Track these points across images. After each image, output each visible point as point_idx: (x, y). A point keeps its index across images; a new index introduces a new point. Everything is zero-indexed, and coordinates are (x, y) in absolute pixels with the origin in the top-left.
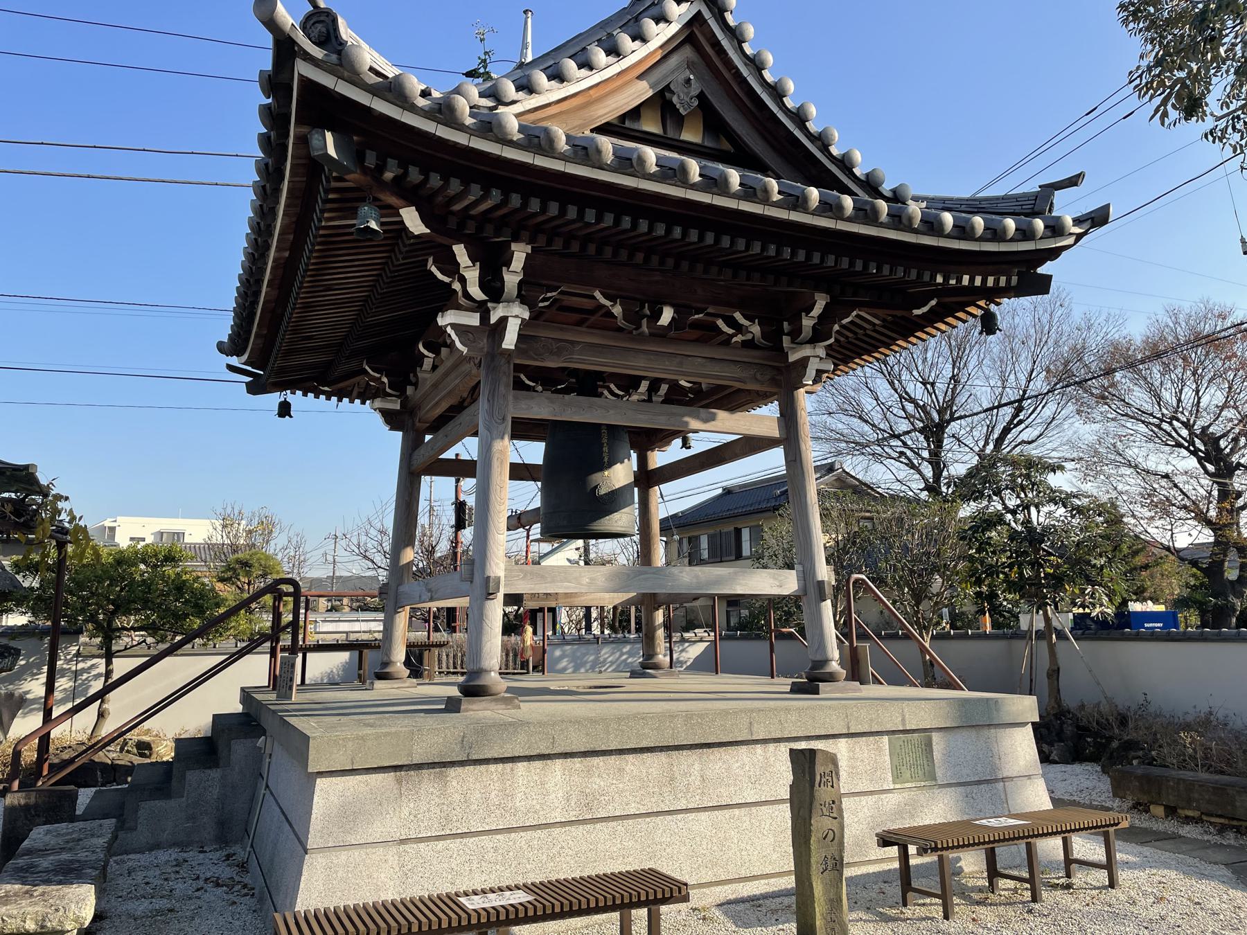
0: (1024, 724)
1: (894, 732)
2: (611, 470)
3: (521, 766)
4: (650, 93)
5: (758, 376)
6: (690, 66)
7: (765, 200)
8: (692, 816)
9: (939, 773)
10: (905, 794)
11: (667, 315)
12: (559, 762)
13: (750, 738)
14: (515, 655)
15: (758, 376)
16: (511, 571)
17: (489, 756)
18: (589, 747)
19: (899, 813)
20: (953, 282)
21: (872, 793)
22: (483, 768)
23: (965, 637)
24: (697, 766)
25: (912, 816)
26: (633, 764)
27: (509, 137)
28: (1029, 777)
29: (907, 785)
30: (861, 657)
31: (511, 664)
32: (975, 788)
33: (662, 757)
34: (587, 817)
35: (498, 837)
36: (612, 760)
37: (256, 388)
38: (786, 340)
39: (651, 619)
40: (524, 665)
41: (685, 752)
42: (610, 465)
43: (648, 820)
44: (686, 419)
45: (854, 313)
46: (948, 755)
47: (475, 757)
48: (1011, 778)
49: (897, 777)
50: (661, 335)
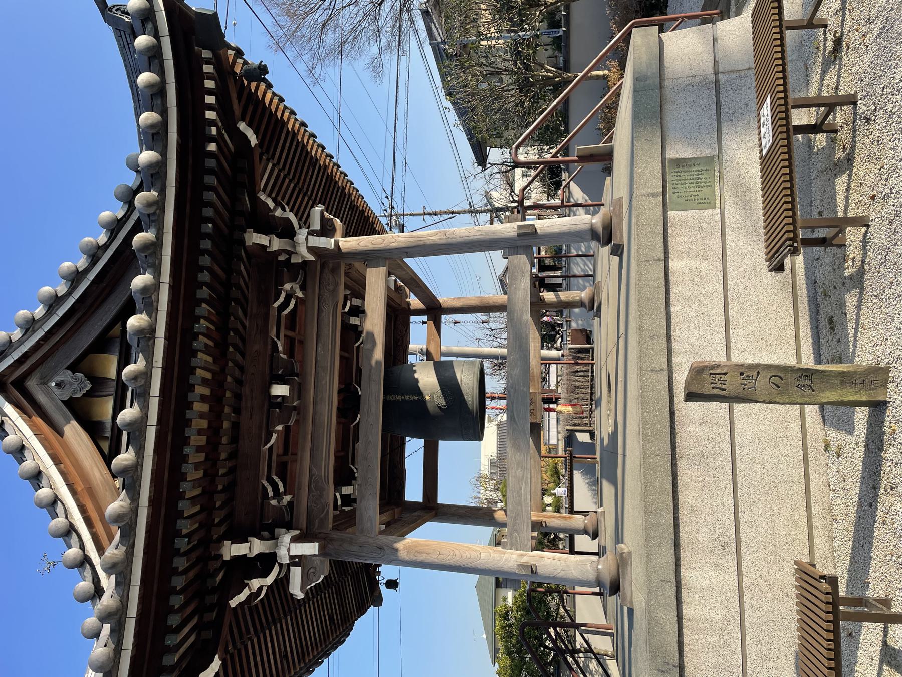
0: (660, 37)
1: (665, 204)
2: (425, 392)
3: (686, 611)
4: (74, 423)
5: (331, 287)
6: (44, 381)
7: (146, 375)
8: (738, 439)
9: (706, 152)
10: (727, 195)
11: (280, 390)
12: (683, 573)
13: (666, 373)
14: (579, 358)
15: (331, 287)
16: (512, 544)
17: (676, 646)
18: (671, 545)
19: (745, 205)
20: (214, 131)
21: (723, 234)
22: (686, 649)
23: (567, 17)
24: (691, 428)
25: (749, 189)
26: (687, 495)
27: (112, 655)
28: (715, 40)
29: (717, 189)
30: (587, 153)
31: (585, 361)
32: (724, 110)
33: (681, 464)
34: (734, 548)
35: (748, 639)
36: (683, 517)
37: (378, 601)
38: (294, 260)
39: (551, 305)
40: (586, 351)
41: (678, 440)
42: (419, 392)
43: (739, 485)
44: (373, 363)
45: (263, 197)
46: (688, 139)
47: (677, 660)
48: (716, 63)
49: (707, 203)
50: (299, 390)
